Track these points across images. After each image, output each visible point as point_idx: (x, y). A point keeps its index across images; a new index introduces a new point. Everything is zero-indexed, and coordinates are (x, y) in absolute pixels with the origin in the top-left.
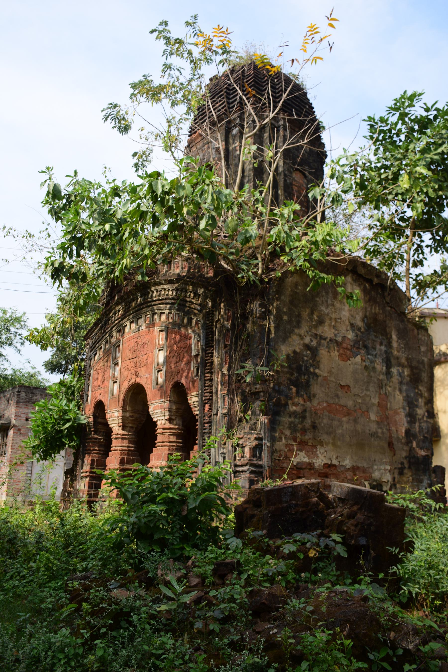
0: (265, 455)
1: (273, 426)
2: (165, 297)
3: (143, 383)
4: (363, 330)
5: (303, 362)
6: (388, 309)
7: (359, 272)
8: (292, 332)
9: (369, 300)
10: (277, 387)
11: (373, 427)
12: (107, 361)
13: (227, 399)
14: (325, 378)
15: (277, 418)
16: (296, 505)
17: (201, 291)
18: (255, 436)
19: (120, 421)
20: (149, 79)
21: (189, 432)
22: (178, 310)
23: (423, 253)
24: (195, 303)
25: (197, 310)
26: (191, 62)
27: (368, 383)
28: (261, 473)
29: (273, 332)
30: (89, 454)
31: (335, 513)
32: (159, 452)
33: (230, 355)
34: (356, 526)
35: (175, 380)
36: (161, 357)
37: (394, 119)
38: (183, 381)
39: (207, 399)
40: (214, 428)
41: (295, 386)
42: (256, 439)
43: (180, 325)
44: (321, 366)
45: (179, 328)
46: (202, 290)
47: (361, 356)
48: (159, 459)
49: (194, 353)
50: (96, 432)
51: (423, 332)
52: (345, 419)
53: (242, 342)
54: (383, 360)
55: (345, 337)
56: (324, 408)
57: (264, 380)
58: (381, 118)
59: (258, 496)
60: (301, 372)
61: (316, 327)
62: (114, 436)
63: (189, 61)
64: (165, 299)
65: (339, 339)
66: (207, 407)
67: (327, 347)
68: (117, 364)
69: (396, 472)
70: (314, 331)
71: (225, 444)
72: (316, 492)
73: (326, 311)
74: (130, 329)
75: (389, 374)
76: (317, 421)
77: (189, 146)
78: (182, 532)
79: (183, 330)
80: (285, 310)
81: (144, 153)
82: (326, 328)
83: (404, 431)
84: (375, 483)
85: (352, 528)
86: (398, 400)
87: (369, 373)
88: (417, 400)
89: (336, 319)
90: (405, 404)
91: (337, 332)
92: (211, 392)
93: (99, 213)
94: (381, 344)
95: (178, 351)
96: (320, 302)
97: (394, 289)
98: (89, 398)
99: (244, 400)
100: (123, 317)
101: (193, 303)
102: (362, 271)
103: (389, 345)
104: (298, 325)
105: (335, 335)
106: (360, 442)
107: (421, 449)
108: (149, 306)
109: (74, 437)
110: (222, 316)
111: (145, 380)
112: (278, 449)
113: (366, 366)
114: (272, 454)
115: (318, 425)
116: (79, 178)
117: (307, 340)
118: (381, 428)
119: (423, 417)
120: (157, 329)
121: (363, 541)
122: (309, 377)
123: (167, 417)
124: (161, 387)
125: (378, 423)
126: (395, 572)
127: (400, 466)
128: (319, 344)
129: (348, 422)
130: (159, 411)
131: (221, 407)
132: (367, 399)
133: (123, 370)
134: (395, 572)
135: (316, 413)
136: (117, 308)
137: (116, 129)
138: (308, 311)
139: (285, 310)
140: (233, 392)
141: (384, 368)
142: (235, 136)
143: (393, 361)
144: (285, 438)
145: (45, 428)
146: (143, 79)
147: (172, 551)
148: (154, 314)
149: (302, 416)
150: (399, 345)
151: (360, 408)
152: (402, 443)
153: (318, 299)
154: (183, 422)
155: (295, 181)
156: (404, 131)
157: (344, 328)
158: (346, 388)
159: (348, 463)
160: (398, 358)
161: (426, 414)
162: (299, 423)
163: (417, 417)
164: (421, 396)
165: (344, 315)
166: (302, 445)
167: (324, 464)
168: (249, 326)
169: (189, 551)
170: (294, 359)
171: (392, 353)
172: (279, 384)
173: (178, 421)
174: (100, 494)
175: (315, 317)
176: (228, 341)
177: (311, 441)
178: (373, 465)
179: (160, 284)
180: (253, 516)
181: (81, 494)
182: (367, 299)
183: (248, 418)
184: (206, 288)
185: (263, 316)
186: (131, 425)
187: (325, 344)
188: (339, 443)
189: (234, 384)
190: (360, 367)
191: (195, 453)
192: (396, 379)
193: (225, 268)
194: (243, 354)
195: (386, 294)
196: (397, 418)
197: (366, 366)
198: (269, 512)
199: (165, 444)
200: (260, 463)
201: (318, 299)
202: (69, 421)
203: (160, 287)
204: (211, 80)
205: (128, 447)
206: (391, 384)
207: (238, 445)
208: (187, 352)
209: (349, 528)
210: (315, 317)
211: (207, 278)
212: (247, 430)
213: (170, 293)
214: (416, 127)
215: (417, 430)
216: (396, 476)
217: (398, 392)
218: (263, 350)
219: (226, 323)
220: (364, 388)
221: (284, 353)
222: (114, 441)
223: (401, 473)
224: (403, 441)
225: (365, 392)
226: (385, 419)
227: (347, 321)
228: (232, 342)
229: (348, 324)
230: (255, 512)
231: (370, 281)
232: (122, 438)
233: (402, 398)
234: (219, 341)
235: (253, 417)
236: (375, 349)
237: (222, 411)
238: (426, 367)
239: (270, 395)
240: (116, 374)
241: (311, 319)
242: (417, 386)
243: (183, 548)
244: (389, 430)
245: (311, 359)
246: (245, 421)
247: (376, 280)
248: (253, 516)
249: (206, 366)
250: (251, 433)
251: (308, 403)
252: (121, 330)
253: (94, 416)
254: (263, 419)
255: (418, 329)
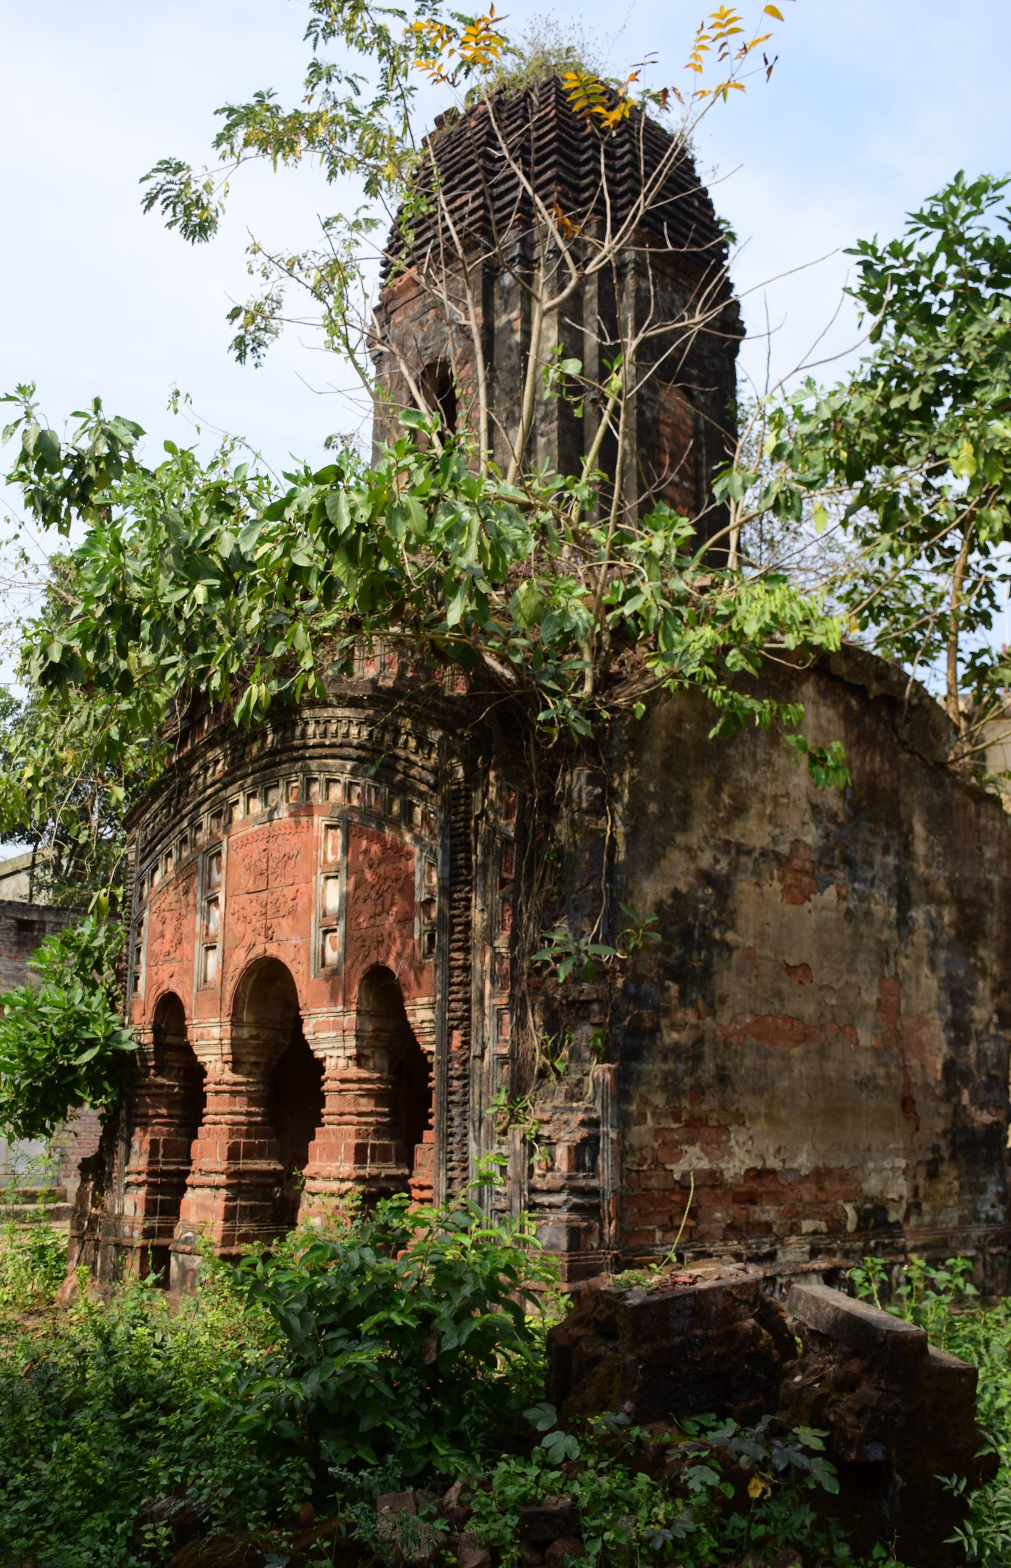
0: (605, 1163)
1: (623, 1086)
2: (339, 740)
3: (286, 959)
4: (841, 818)
5: (696, 916)
6: (905, 757)
7: (835, 672)
8: (668, 842)
9: (858, 741)
10: (632, 989)
11: (866, 1063)
12: (186, 892)
13: (507, 1018)
14: (750, 953)
15: (634, 1065)
16: (705, 1339)
17: (435, 736)
18: (581, 1116)
19: (227, 1049)
20: (270, 102)
21: (408, 1094)
22: (376, 778)
23: (990, 595)
24: (422, 765)
25: (427, 783)
26: (383, 53)
27: (855, 952)
28: (597, 1208)
29: (622, 847)
30: (145, 1126)
31: (803, 1369)
32: (333, 1140)
33: (514, 908)
34: (860, 1414)
35: (372, 960)
36: (332, 895)
37: (928, 246)
38: (391, 963)
39: (457, 1019)
40: (475, 1090)
41: (676, 981)
42: (583, 1123)
43: (383, 819)
44: (740, 922)
45: (380, 827)
46: (440, 733)
47: (838, 886)
48: (332, 1156)
49: (421, 896)
50: (160, 1070)
51: (991, 809)
52: (796, 1051)
53: (544, 876)
54: (889, 890)
55: (797, 841)
56: (747, 1028)
57: (600, 972)
58: (891, 245)
59: (608, 1312)
60: (691, 944)
61: (727, 823)
62: (211, 1087)
63: (376, 52)
64: (341, 746)
65: (784, 849)
66: (457, 1037)
67: (754, 873)
68: (214, 901)
69: (922, 1171)
70: (722, 834)
71: (504, 1133)
72: (753, 1305)
73: (752, 782)
74: (247, 812)
75: (906, 924)
76: (729, 1064)
77: (384, 310)
78: (424, 1407)
79: (388, 833)
80: (652, 788)
81: (259, 308)
82: (752, 824)
83: (939, 1066)
84: (868, 1206)
85: (850, 1419)
86: (927, 987)
87: (856, 928)
88: (973, 986)
89: (775, 799)
90: (944, 997)
91: (777, 831)
92: (467, 1001)
93: (176, 553)
94: (886, 851)
95: (376, 888)
96: (738, 758)
97: (920, 705)
98: (141, 983)
99: (551, 1026)
100: (228, 780)
101: (414, 764)
102: (842, 668)
103: (906, 851)
104: (685, 827)
105: (775, 840)
106: (833, 1107)
107: (982, 1106)
108: (296, 760)
109: (106, 1085)
110: (491, 803)
111: (292, 952)
112: (636, 1144)
113: (848, 911)
114: (623, 1159)
115: (732, 1074)
116: (108, 414)
117: (705, 860)
118: (886, 1065)
119: (987, 1026)
120: (319, 821)
121: (876, 1453)
122: (710, 953)
123: (353, 1052)
124: (335, 972)
125: (876, 1052)
126: (961, 1542)
127: (930, 1156)
128: (734, 867)
129: (804, 1059)
130: (331, 1034)
131: (494, 1039)
132: (852, 994)
133: (230, 919)
134: (961, 1542)
135: (727, 1044)
136: (210, 755)
137: (176, 228)
138: (707, 785)
139: (652, 788)
140: (523, 1001)
141: (894, 911)
142: (508, 291)
143: (915, 890)
144: (653, 1114)
145: (29, 1060)
146: (253, 101)
147: (405, 1457)
148: (310, 781)
149: (693, 1054)
150: (931, 848)
151: (834, 1020)
152: (935, 1098)
153: (732, 752)
154: (391, 1061)
155: (666, 410)
156: (951, 280)
157: (797, 819)
158: (800, 971)
159: (803, 1162)
160: (927, 883)
161: (995, 1019)
162: (686, 1073)
163: (973, 1026)
164: (983, 972)
165: (796, 786)
166: (695, 1127)
167: (748, 1171)
168: (562, 829)
169: (449, 1459)
170: (675, 912)
171: (912, 870)
172: (637, 979)
173: (379, 1060)
174: (178, 1232)
175: (726, 799)
176: (508, 870)
177: (715, 1116)
178: (864, 1160)
179: (326, 705)
180: (597, 1360)
181: (127, 1229)
182: (852, 737)
183: (560, 1066)
184: (449, 729)
185: (598, 808)
186: (253, 1059)
187: (750, 865)
188: (783, 1113)
189: (526, 984)
190: (834, 915)
191: (427, 1151)
192: (921, 935)
193: (495, 672)
194: (546, 901)
195: (900, 721)
196: (924, 1034)
197: (848, 911)
198: (640, 1359)
199: (346, 1118)
200: (594, 1183)
201: (732, 752)
202: (91, 1043)
203: (326, 713)
204: (439, 121)
205: (248, 1114)
206: (909, 950)
207: (538, 1138)
208: (401, 890)
209: (841, 1418)
210: (726, 799)
211: (450, 700)
212: (559, 1101)
213: (354, 731)
214: (985, 270)
215: (973, 1060)
216: (921, 1181)
217: (926, 970)
218: (597, 895)
219: (502, 822)
220: (844, 967)
221: (650, 899)
222: (210, 1098)
223: (933, 1174)
224: (938, 1091)
225: (845, 977)
226: (895, 1042)
227: (804, 800)
228: (518, 873)
229: (804, 805)
230: (602, 1350)
231: (860, 691)
232: (231, 1092)
233: (935, 984)
234: (484, 866)
235: (573, 1066)
236: (870, 864)
237: (497, 1048)
238: (997, 898)
239: (615, 1009)
240: (211, 926)
241: (716, 804)
242: (975, 948)
243: (430, 1448)
244: (904, 1068)
245: (715, 906)
246: (553, 1077)
247: (875, 689)
248: (597, 1360)
249: (451, 931)
250: (572, 1110)
251: (708, 1020)
252: (222, 813)
253: (156, 1030)
254: (599, 1071)
255: (977, 802)
